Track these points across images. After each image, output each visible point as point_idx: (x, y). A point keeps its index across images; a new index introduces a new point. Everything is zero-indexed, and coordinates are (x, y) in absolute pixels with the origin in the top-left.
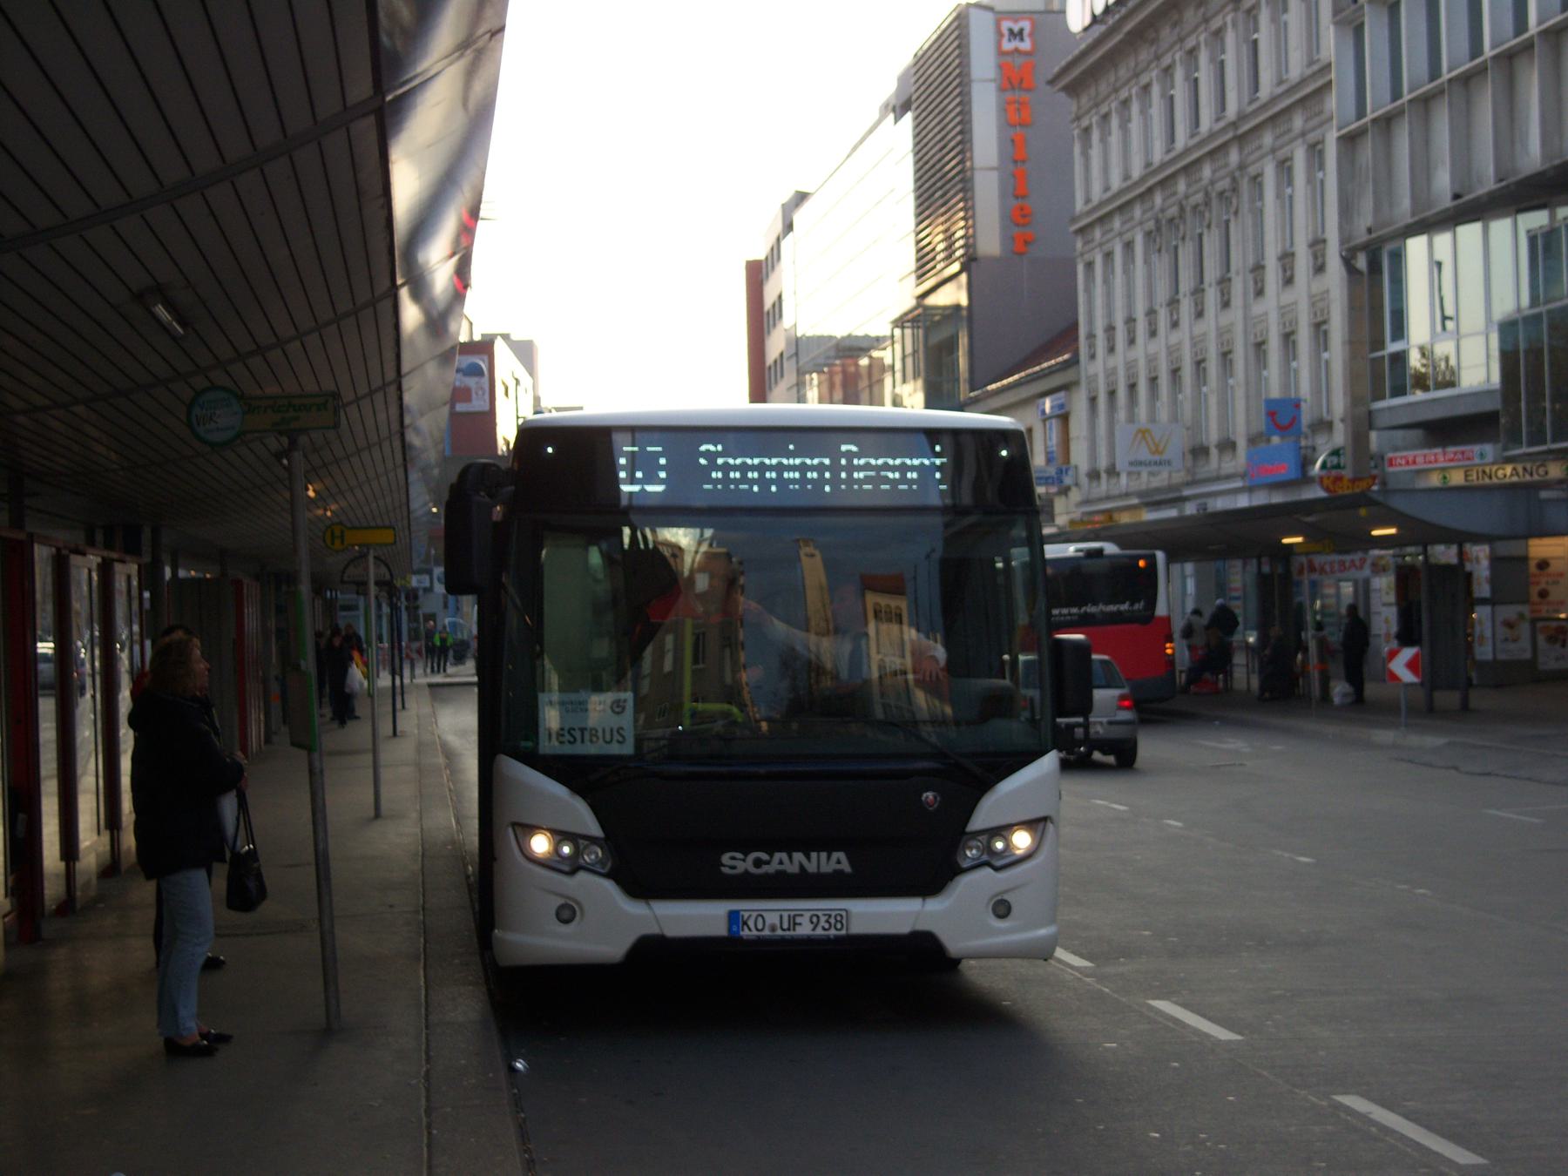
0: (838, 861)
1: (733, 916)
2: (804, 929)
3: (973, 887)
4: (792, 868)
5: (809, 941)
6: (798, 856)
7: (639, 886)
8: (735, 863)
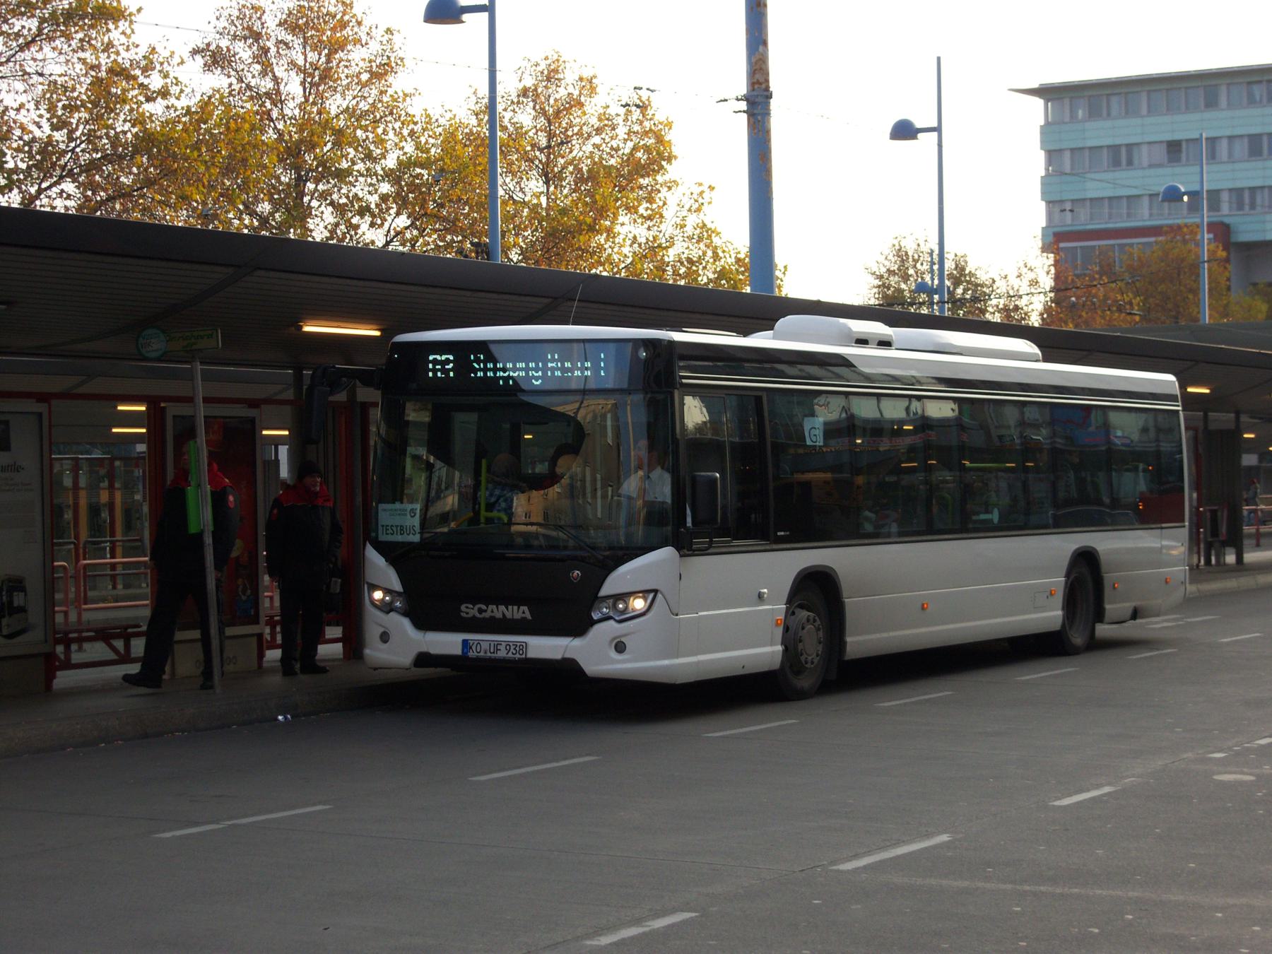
0: (520, 612)
1: (465, 642)
2: (502, 654)
3: (603, 632)
4: (499, 615)
5: (504, 660)
6: (502, 608)
7: (423, 622)
8: (469, 610)
